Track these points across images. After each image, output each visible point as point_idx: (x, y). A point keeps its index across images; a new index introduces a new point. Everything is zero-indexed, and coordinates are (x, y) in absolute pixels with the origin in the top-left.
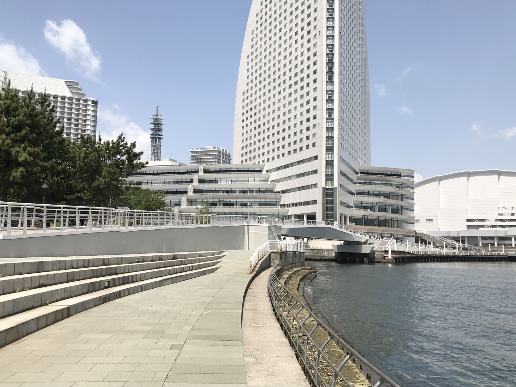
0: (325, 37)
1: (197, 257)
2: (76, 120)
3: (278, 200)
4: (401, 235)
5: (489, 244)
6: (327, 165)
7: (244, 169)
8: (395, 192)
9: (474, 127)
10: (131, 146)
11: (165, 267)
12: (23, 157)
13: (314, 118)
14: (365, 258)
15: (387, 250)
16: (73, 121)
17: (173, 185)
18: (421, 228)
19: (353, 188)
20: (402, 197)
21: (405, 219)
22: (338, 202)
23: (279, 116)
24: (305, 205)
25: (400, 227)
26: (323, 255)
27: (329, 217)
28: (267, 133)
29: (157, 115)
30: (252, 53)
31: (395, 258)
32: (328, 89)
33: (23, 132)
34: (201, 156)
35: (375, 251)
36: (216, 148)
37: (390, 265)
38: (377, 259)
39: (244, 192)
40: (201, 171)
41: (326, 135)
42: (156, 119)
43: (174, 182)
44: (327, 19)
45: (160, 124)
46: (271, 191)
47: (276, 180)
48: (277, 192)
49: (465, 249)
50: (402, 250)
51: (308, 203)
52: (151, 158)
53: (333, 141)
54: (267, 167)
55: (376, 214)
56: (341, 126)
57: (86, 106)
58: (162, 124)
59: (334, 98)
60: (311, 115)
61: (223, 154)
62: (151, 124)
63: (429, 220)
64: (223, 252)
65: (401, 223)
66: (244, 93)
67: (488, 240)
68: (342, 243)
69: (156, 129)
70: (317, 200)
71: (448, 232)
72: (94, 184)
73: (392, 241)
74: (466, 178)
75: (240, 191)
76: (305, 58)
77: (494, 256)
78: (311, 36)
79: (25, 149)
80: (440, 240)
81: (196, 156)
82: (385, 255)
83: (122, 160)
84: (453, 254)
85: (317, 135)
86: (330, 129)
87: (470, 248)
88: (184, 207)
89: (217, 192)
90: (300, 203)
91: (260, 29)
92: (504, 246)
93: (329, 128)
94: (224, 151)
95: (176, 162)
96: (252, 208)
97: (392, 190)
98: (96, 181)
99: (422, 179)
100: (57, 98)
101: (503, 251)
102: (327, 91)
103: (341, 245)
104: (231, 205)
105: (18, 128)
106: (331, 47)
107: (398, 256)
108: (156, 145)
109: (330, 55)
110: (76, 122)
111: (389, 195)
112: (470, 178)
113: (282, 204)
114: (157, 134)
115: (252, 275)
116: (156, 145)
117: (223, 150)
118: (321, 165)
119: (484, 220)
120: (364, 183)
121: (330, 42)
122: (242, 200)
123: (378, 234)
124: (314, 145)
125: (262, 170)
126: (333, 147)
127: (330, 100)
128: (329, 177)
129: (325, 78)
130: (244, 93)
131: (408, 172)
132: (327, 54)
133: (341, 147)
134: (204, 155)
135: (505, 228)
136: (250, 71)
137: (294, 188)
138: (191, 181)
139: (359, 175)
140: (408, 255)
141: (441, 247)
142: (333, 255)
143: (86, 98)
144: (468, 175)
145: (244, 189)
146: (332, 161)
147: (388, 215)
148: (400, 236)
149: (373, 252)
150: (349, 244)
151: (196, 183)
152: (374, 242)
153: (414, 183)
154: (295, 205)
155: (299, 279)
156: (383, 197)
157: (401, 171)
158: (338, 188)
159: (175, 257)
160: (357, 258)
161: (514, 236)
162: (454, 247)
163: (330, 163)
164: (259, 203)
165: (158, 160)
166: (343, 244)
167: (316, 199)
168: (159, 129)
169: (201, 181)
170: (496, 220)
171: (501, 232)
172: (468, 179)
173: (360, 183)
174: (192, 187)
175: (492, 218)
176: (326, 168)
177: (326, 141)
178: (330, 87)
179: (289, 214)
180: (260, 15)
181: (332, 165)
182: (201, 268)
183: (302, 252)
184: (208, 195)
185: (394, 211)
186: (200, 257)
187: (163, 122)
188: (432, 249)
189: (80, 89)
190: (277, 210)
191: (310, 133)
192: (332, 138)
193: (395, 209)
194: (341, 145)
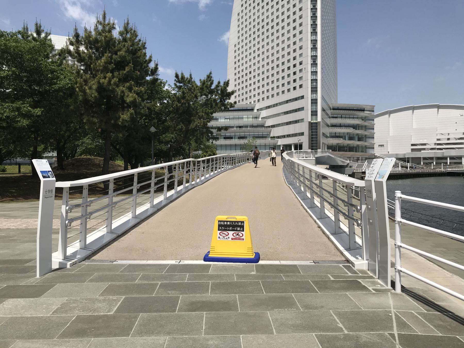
3: (268, 133)
6: (312, 103)
7: (243, 109)
10: (224, 84)
12: (130, 97)
20: (366, 128)
23: (268, 64)
24: (292, 137)
27: (314, 146)
28: (257, 78)
30: (239, 43)
32: (312, 39)
33: (127, 69)
35: (355, 172)
39: (240, 127)
41: (311, 78)
46: (262, 126)
47: (266, 117)
48: (267, 127)
53: (317, 83)
54: (258, 106)
59: (317, 46)
60: (297, 62)
72: (192, 126)
74: (411, 111)
75: (237, 127)
76: (291, 13)
79: (130, 89)
82: (363, 176)
83: (215, 100)
86: (314, 73)
101: (442, 168)
102: (311, 40)
104: (230, 138)
112: (415, 111)
113: (272, 136)
118: (307, 103)
119: (425, 144)
120: (336, 117)
122: (239, 134)
124: (301, 86)
126: (316, 88)
127: (314, 48)
128: (314, 113)
129: (310, 30)
131: (370, 107)
132: (311, 9)
135: (442, 150)
144: (412, 109)
145: (240, 125)
146: (316, 100)
147: (355, 143)
150: (334, 168)
152: (353, 165)
154: (284, 137)
156: (352, 128)
157: (364, 107)
158: (321, 122)
163: (314, 102)
170: (435, 144)
171: (439, 153)
172: (413, 112)
176: (311, 106)
177: (312, 83)
179: (279, 144)
181: (316, 103)
185: (359, 139)
192: (316, 80)
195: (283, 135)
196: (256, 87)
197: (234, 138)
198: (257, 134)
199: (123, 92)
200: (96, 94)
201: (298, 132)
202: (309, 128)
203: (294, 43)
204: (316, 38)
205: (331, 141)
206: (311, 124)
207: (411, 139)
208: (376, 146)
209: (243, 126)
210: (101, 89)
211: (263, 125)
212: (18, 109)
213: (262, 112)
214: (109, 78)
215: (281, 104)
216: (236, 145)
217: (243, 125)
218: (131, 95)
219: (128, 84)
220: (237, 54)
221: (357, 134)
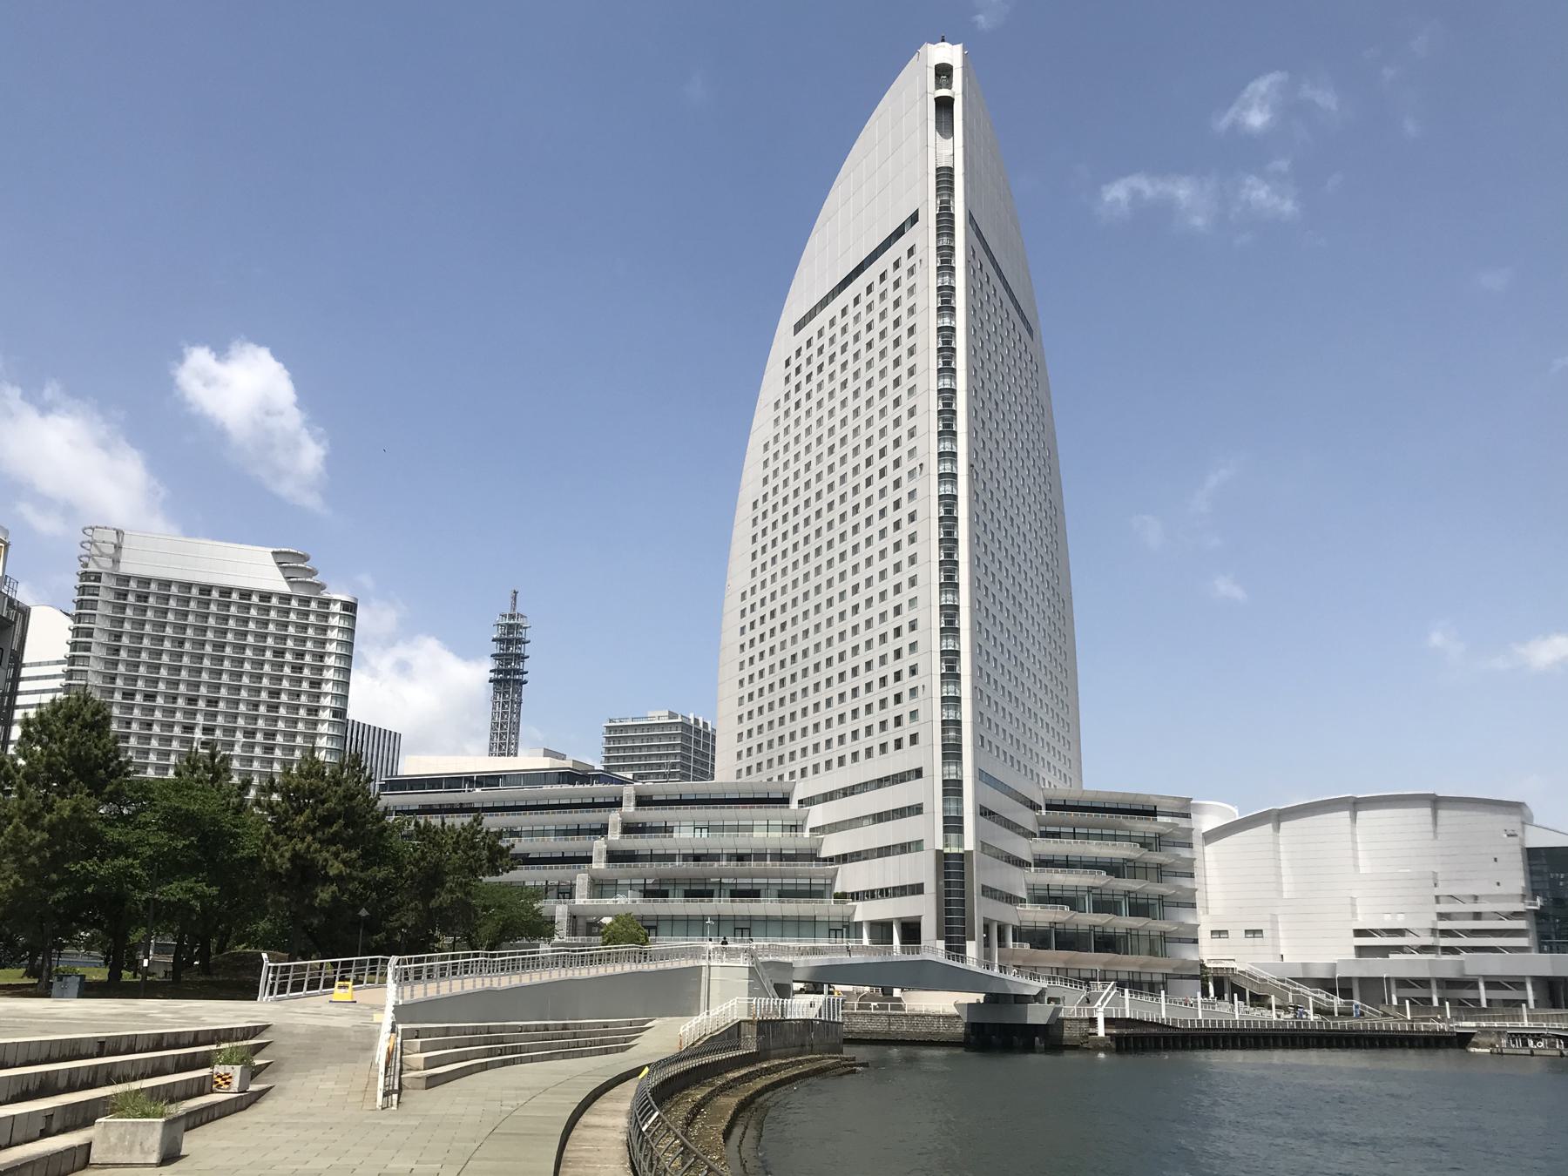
0: (935, 479)
2: (297, 654)
3: (828, 882)
4: (1127, 973)
6: (945, 793)
8: (1139, 858)
9: (1436, 639)
11: (553, 1040)
12: (335, 868)
14: (1037, 1039)
16: (288, 657)
17: (555, 840)
18: (1210, 953)
19: (1024, 848)
20: (1161, 872)
21: (1168, 932)
22: (976, 889)
24: (894, 896)
25: (1156, 955)
26: (934, 1029)
27: (954, 931)
29: (512, 617)
30: (753, 589)
31: (1117, 1039)
33: (335, 828)
34: (633, 738)
35: (1063, 1020)
36: (675, 716)
37: (1102, 1055)
38: (1070, 1040)
39: (741, 858)
40: (629, 799)
42: (510, 626)
43: (557, 832)
44: (939, 436)
45: (520, 641)
46: (812, 856)
47: (823, 826)
48: (825, 860)
50: (1135, 1014)
51: (901, 891)
52: (491, 749)
53: (959, 731)
54: (802, 790)
55: (1088, 919)
56: (981, 691)
57: (326, 616)
58: (527, 639)
61: (698, 732)
62: (494, 640)
64: (651, 1020)
65: (1159, 944)
66: (744, 595)
67: (1414, 987)
68: (981, 997)
71: (1305, 965)
72: (433, 904)
75: (730, 857)
77: (1378, 1031)
78: (902, 472)
79: (336, 855)
80: (1282, 987)
81: (619, 739)
82: (1091, 1031)
85: (921, 714)
86: (952, 702)
88: (581, 900)
89: (670, 858)
90: (882, 890)
92: (1479, 1000)
93: (950, 699)
94: (701, 725)
95: (563, 757)
96: (760, 902)
97: (1129, 853)
98: (436, 897)
99: (1237, 814)
100: (250, 595)
101: (1526, 1018)
103: (978, 1003)
105: (327, 821)
106: (949, 501)
107: (1125, 1031)
109: (948, 520)
110: (297, 659)
112: (1361, 814)
113: (839, 891)
114: (511, 670)
117: (696, 721)
118: (929, 792)
119: (1399, 932)
121: (948, 489)
123: (1055, 971)
124: (914, 739)
125: (788, 799)
126: (959, 747)
128: (953, 825)
129: (936, 577)
130: (744, 595)
133: (982, 745)
134: (642, 738)
138: (603, 831)
139: (1044, 812)
140: (1154, 1031)
142: (961, 1029)
143: (325, 595)
145: (739, 851)
146: (959, 783)
147: (1123, 922)
148: (1158, 978)
149: (1057, 1023)
151: (614, 835)
154: (871, 895)
156: (1104, 874)
157: (1155, 801)
158: (974, 853)
159: (565, 1027)
161: (1484, 976)
163: (952, 789)
165: (509, 754)
166: (982, 1001)
169: (629, 829)
170: (1433, 931)
171: (1446, 966)
172: (1354, 819)
173: (1045, 835)
174: (605, 846)
175: (1420, 920)
177: (943, 731)
178: (949, 599)
179: (857, 918)
180: (794, 364)
181: (960, 793)
184: (647, 867)
187: (528, 635)
189: (312, 573)
190: (825, 908)
192: (958, 723)
194: (980, 741)
195: (868, 889)
197: (716, 893)
198: (793, 881)
199: (326, 860)
200: (288, 865)
201: (908, 883)
204: (954, 601)
205: (1027, 914)
208: (1204, 935)
209: (750, 855)
210: (296, 856)
211: (814, 852)
212: (191, 890)
213: (812, 808)
214: (308, 844)
215: (864, 787)
216: (719, 920)
217: (749, 851)
218: (336, 864)
219: (333, 849)
221: (1127, 893)
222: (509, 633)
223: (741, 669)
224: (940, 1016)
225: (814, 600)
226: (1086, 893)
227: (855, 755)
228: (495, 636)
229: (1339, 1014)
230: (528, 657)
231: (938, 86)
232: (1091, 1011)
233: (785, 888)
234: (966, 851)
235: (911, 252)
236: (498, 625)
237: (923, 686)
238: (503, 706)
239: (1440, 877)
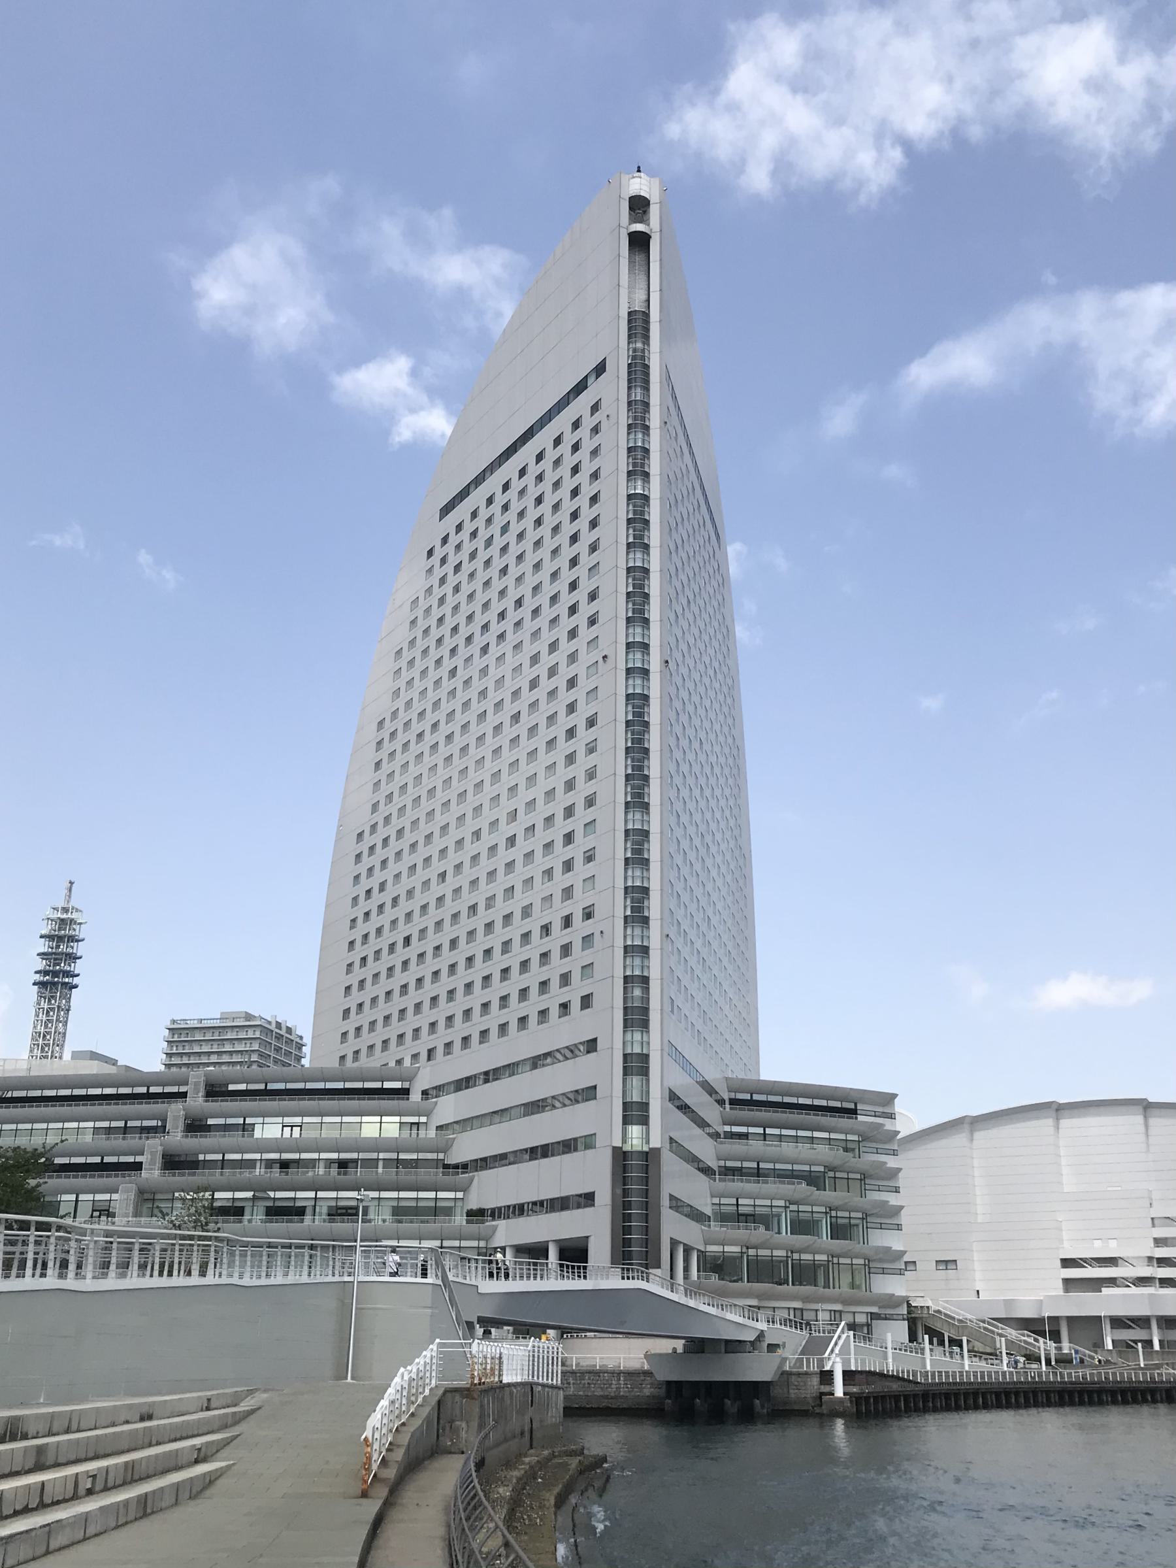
1: (127, 1422)
4: (865, 1315)
5: (1136, 1342)
13: (588, 915)
14: (757, 1402)
15: (827, 1368)
22: (665, 1202)
26: (612, 1391)
29: (65, 910)
30: (374, 828)
42: (62, 920)
45: (73, 939)
48: (456, 1166)
49: (1064, 1361)
50: (856, 1366)
51: (561, 1204)
53: (647, 990)
54: (425, 1079)
58: (81, 937)
61: (279, 1037)
62: (42, 937)
63: (946, 1262)
66: (360, 835)
68: (679, 1345)
69: (58, 954)
70: (593, 1193)
71: (1008, 1303)
73: (844, 1336)
74: (1050, 1122)
77: (1120, 1382)
80: (985, 1329)
84: (908, 1376)
87: (1078, 1356)
91: (420, 644)
108: (53, 1009)
111: (822, 1174)
113: (475, 1207)
114: (60, 971)
115: (372, 1507)
116: (53, 1009)
119: (1111, 1261)
123: (792, 1312)
124: (586, 1001)
125: (409, 1089)
128: (636, 1113)
136: (383, 810)
137: (515, 1152)
140: (895, 1386)
141: (991, 1354)
153: (899, 1137)
154: (519, 1210)
155: (552, 1502)
156: (804, 1185)
160: (729, 1402)
162: (1028, 1353)
164: (395, 1204)
166: (680, 1350)
167: (591, 1190)
168: (67, 955)
172: (1057, 1128)
174: (160, 1148)
182: (136, 1477)
183: (552, 1387)
186: (142, 1419)
188: (967, 1362)
191: (573, 964)
193: (844, 1225)
196: (475, 1004)
202: (614, 1174)
203: (569, 838)
206: (621, 1157)
207: (1061, 1241)
208: (926, 1266)
220: (362, 868)
222: (60, 929)
223: (351, 928)
224: (620, 1373)
225: (386, 960)
226: (783, 1210)
227: (503, 1028)
228: (43, 932)
229: (1057, 1361)
230: (80, 958)
231: (633, 220)
232: (821, 1362)
233: (403, 1204)
234: (650, 1149)
235: (595, 408)
236: (48, 919)
237: (602, 932)
238: (48, 1012)
239: (1155, 1196)
